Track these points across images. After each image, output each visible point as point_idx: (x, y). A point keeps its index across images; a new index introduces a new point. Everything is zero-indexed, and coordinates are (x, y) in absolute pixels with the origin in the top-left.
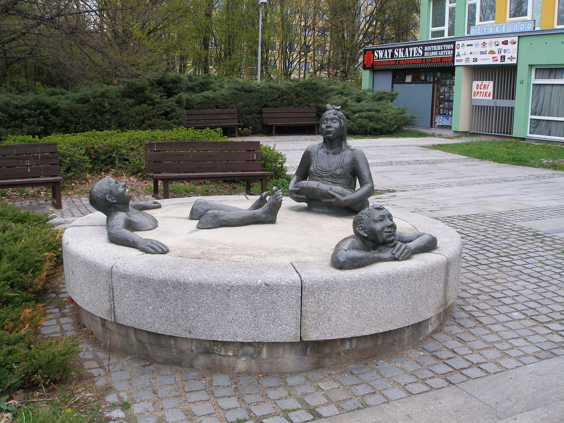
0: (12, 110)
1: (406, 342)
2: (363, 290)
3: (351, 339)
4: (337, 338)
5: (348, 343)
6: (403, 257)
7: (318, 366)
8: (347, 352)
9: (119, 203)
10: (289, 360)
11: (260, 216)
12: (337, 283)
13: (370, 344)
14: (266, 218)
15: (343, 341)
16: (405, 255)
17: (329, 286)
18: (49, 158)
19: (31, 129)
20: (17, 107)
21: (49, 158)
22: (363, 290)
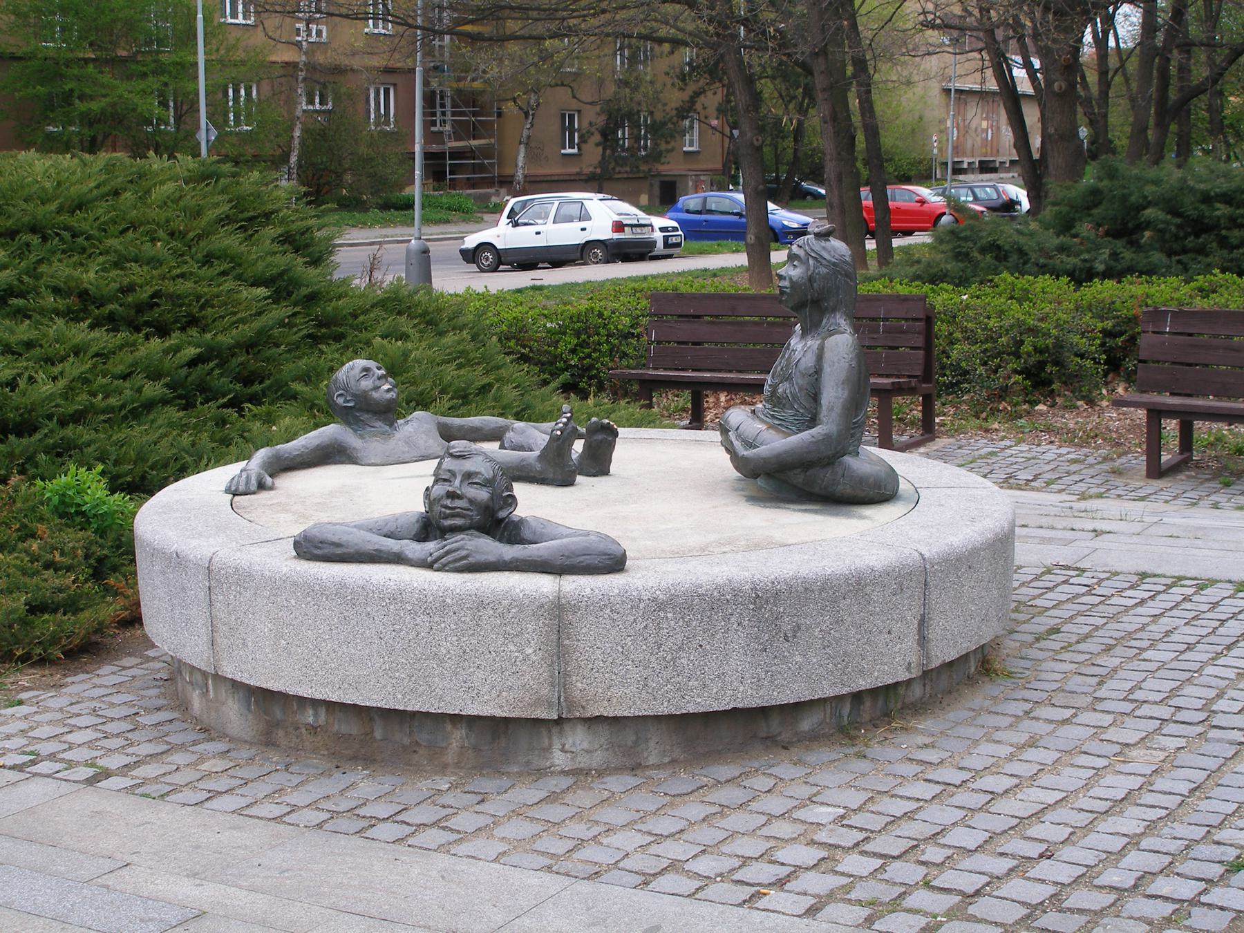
0: (1190, 206)
1: (450, 757)
2: (293, 602)
3: (315, 703)
4: (257, 685)
5: (311, 712)
6: (445, 565)
7: (267, 740)
8: (313, 729)
9: (360, 410)
10: (233, 714)
11: (530, 465)
12: (250, 576)
13: (351, 727)
14: (541, 472)
15: (302, 700)
16: (456, 561)
17: (276, 586)
18: (903, 332)
19: (1231, 261)
20: (1207, 199)
21: (903, 332)
22: (293, 602)
